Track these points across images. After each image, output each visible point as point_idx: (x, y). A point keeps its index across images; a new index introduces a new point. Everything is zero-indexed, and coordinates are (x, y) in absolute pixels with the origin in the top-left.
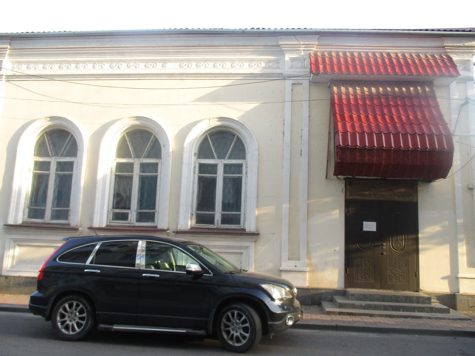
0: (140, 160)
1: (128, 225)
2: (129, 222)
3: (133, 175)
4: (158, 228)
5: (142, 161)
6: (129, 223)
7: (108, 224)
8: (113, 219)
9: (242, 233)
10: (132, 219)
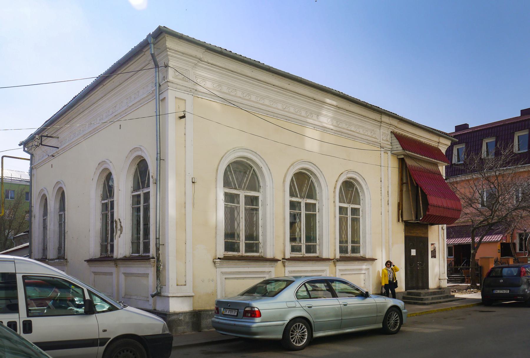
9: (363, 259)
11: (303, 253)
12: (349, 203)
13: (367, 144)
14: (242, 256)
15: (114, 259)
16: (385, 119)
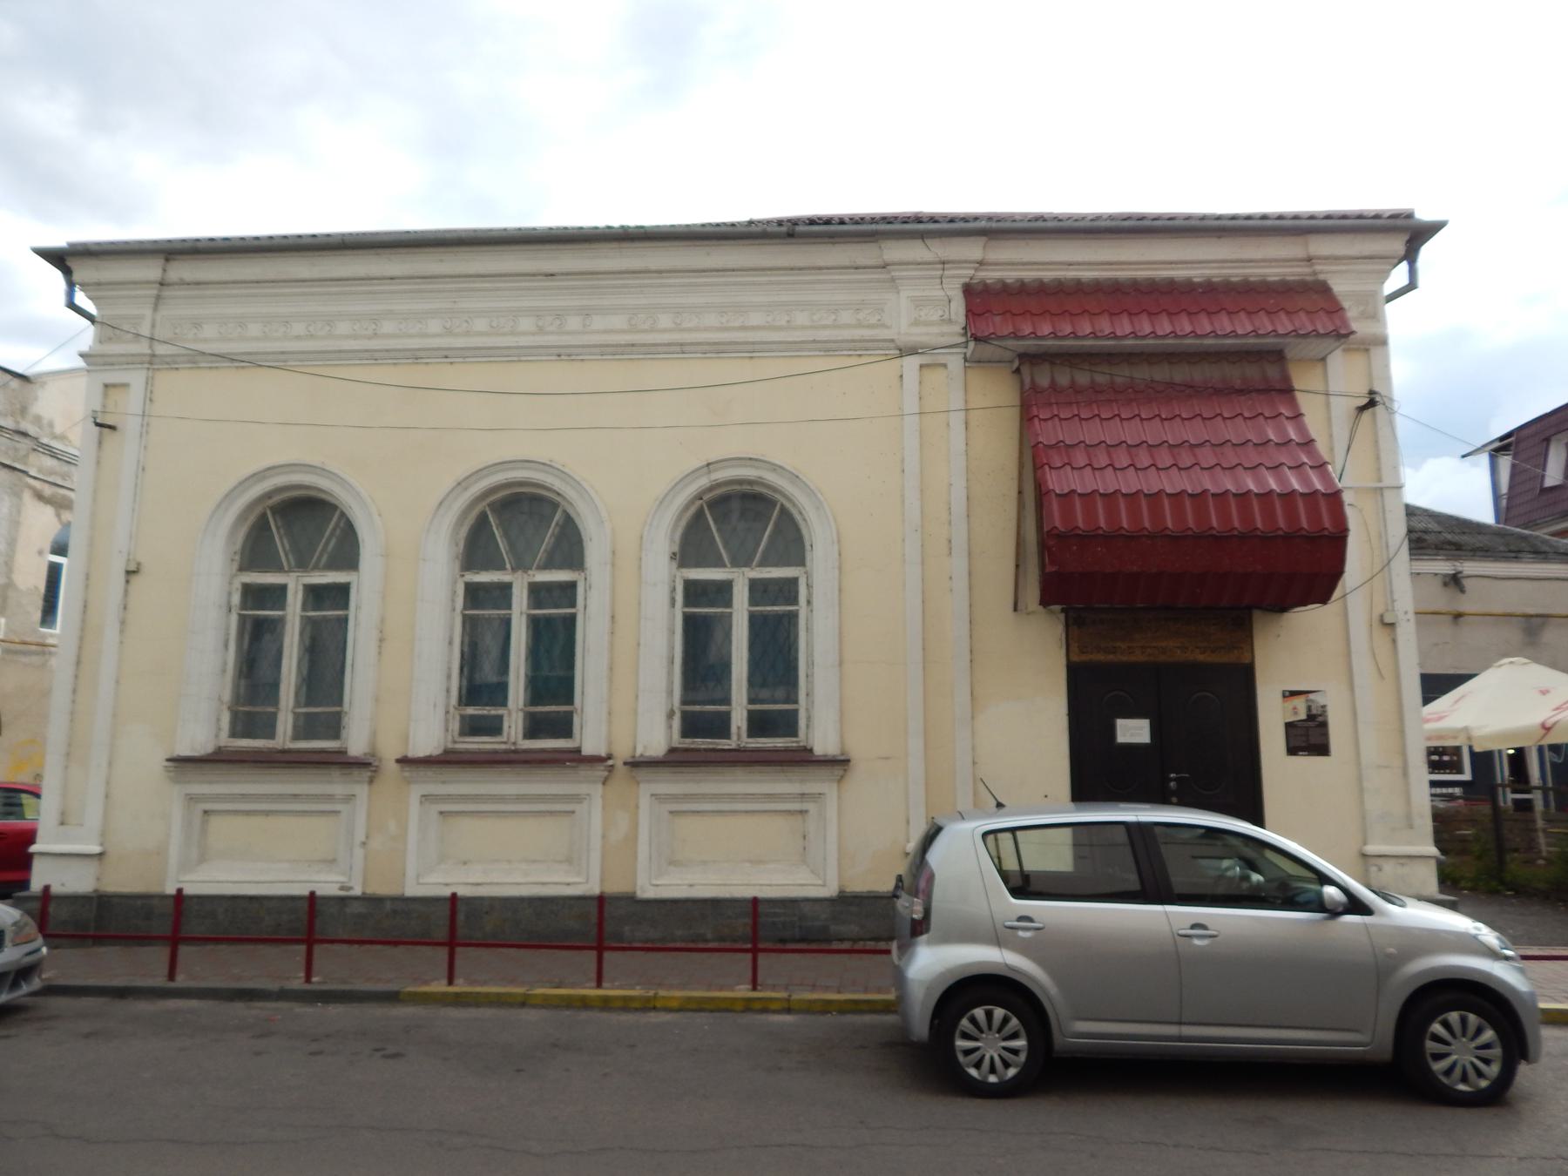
1: (503, 747)
2: (505, 739)
7: (450, 746)
9: (803, 759)
11: (284, 736)
12: (736, 563)
13: (822, 353)
14: (284, 752)
15: (814, 759)
16: (895, 251)
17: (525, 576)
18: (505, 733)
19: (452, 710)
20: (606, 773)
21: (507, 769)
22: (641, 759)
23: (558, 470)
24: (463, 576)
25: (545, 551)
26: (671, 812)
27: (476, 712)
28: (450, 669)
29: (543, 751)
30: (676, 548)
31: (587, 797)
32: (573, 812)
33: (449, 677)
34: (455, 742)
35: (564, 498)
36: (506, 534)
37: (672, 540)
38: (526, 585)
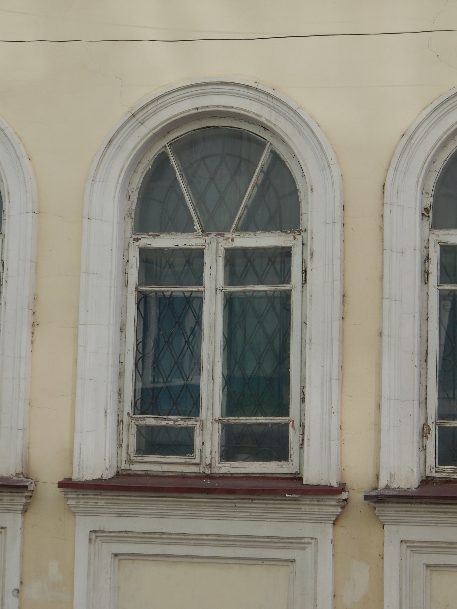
0: (227, 239)
1: (194, 469)
2: (197, 460)
3: (202, 292)
4: (304, 483)
5: (233, 240)
6: (195, 464)
7: (124, 466)
8: (139, 451)
10: (208, 451)
17: (221, 239)
18: (197, 452)
19: (126, 419)
20: (340, 510)
21: (203, 499)
22: (386, 493)
23: (267, 94)
24: (137, 240)
25: (246, 206)
26: (428, 566)
27: (158, 423)
28: (121, 363)
29: (247, 477)
30: (428, 202)
31: (313, 541)
32: (293, 561)
33: (121, 375)
34: (131, 462)
35: (274, 133)
36: (190, 183)
37: (424, 191)
38: (221, 252)
